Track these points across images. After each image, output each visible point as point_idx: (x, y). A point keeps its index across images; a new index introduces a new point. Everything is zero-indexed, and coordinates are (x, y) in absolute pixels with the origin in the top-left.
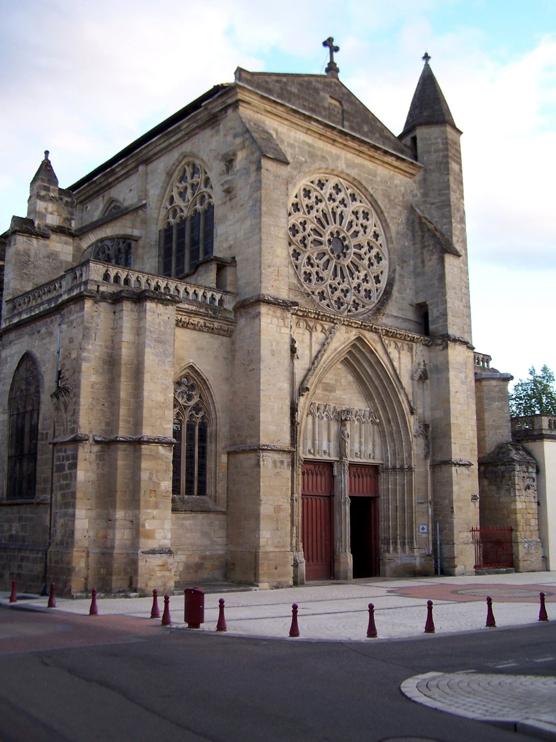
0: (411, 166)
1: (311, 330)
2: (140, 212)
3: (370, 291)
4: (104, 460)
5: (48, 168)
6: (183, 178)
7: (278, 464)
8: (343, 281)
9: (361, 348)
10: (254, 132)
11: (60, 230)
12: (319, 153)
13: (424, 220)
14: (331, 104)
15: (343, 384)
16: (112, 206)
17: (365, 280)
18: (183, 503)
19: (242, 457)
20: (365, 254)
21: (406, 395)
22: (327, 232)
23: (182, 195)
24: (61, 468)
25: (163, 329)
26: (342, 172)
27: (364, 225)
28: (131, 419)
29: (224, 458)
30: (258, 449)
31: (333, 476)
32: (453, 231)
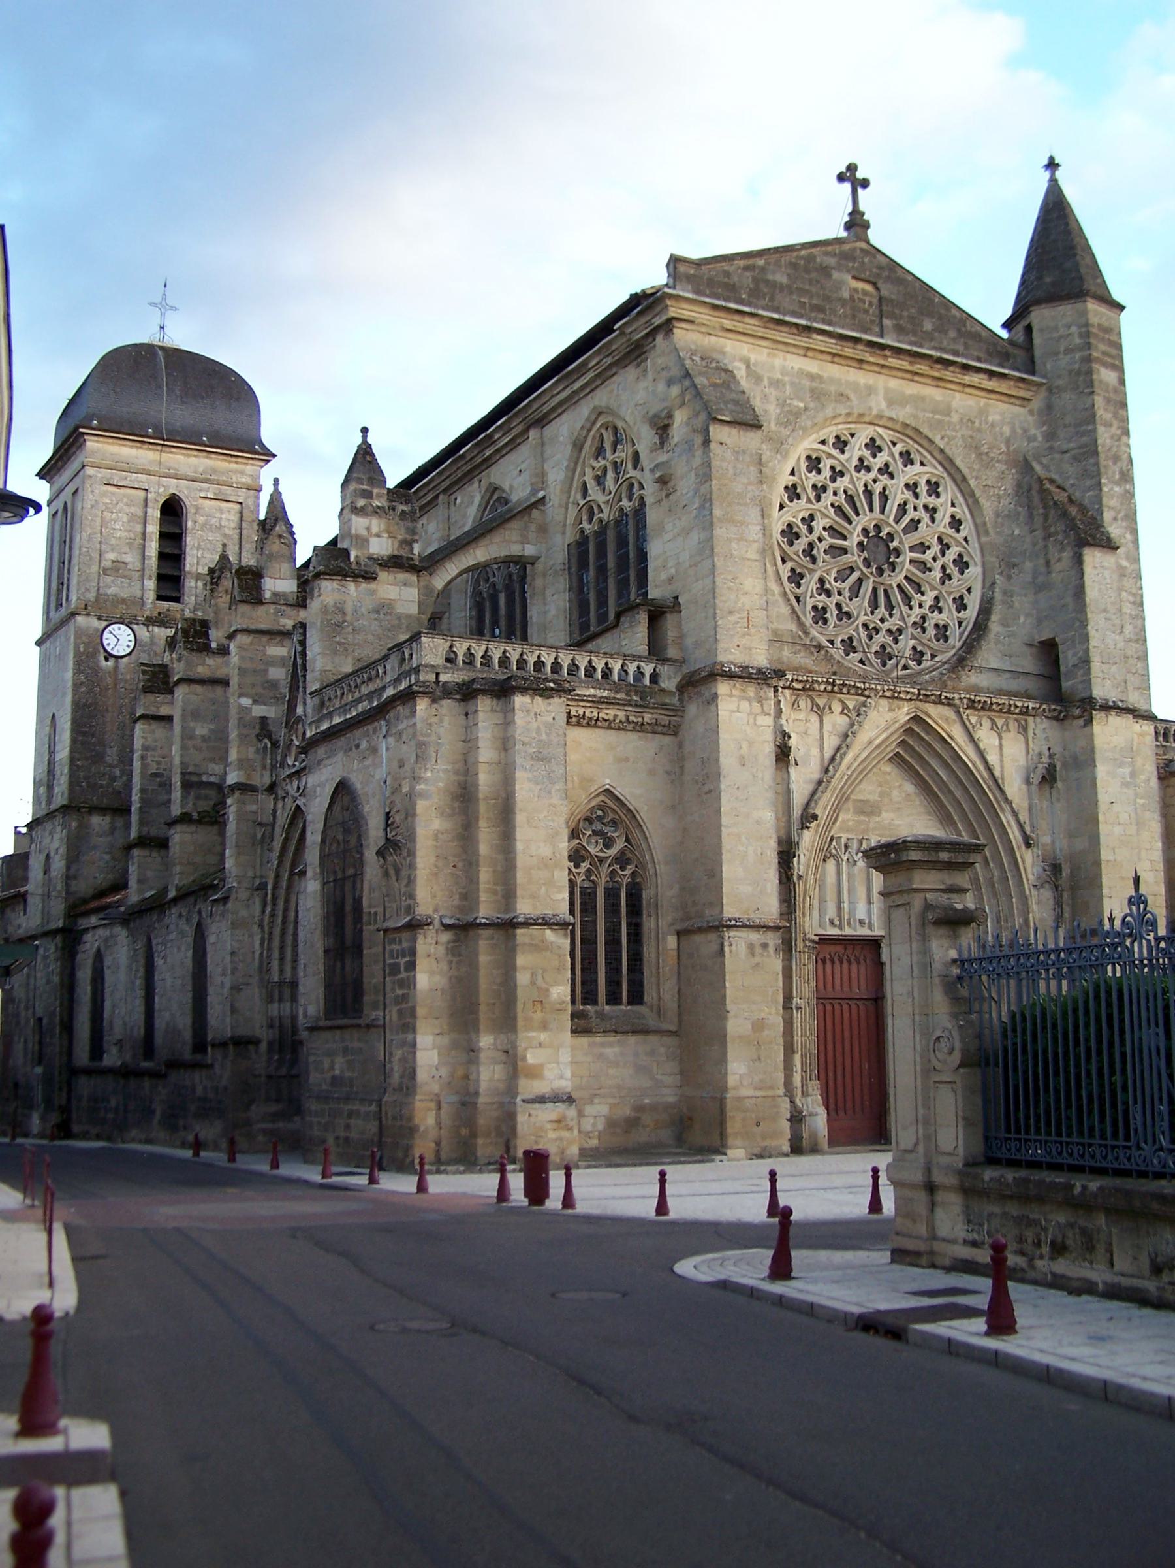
0: (1021, 385)
1: (820, 711)
2: (535, 513)
3: (945, 627)
4: (460, 955)
5: (368, 458)
6: (599, 452)
7: (758, 950)
8: (891, 615)
9: (923, 734)
10: (700, 374)
11: (395, 563)
12: (833, 388)
13: (1048, 486)
14: (856, 290)
15: (896, 799)
16: (495, 497)
17: (936, 607)
18: (602, 1019)
19: (698, 938)
20: (934, 559)
21: (1015, 814)
22: (854, 529)
23: (600, 480)
24: (395, 970)
25: (544, 737)
26: (881, 417)
27: (931, 506)
28: (499, 888)
29: (672, 942)
30: (720, 927)
31: (881, 965)
32: (1105, 500)
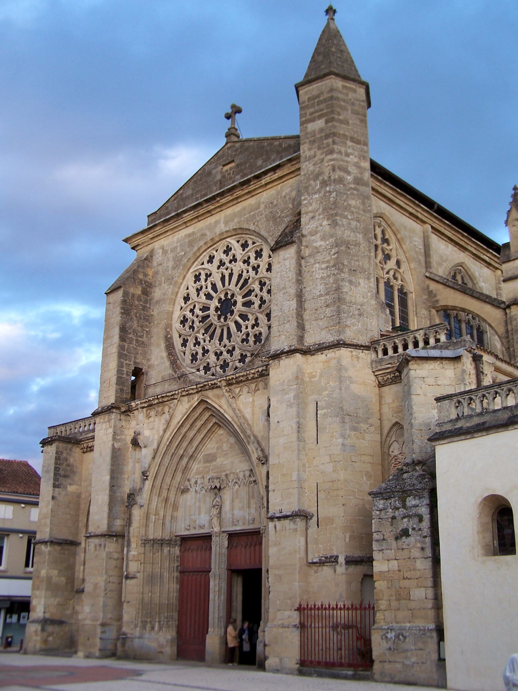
7: (98, 547)
